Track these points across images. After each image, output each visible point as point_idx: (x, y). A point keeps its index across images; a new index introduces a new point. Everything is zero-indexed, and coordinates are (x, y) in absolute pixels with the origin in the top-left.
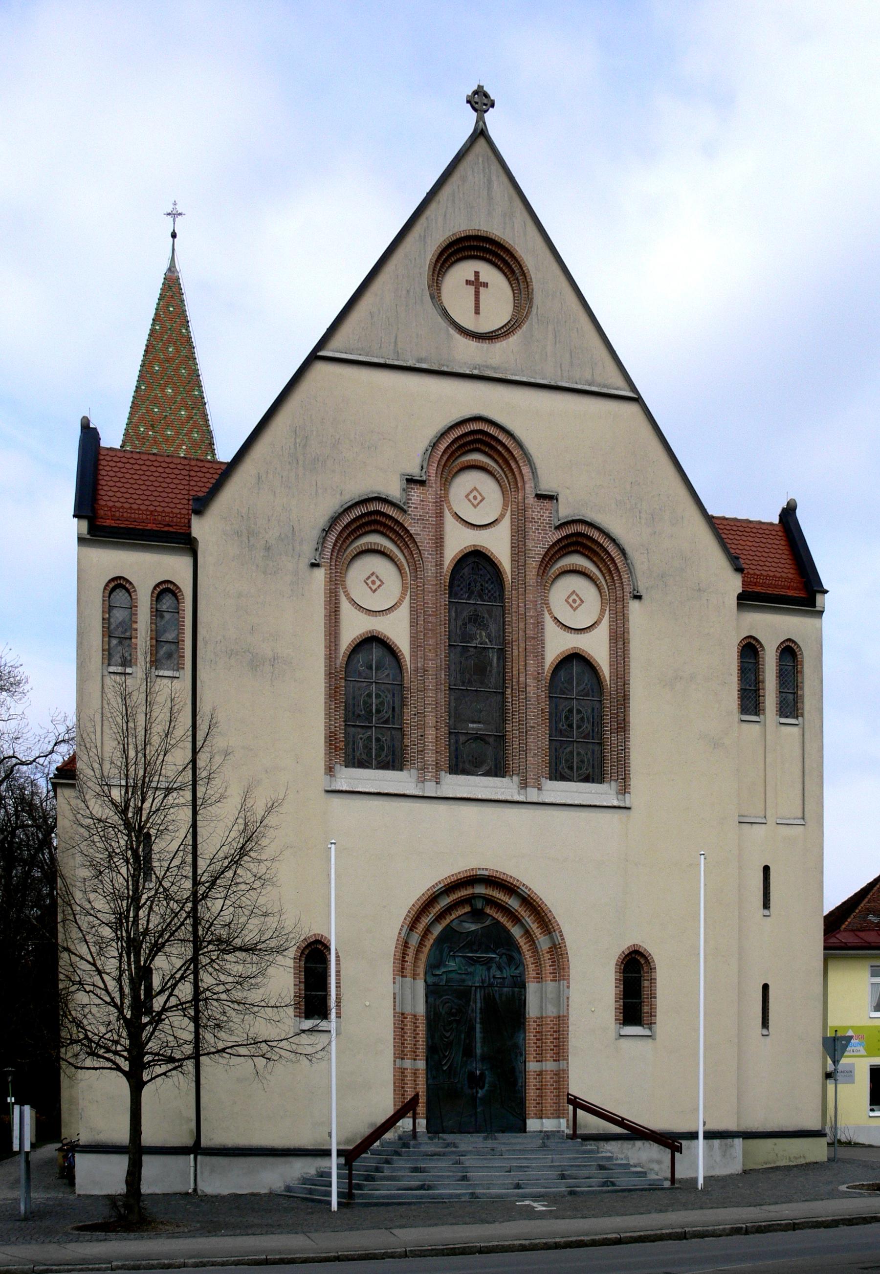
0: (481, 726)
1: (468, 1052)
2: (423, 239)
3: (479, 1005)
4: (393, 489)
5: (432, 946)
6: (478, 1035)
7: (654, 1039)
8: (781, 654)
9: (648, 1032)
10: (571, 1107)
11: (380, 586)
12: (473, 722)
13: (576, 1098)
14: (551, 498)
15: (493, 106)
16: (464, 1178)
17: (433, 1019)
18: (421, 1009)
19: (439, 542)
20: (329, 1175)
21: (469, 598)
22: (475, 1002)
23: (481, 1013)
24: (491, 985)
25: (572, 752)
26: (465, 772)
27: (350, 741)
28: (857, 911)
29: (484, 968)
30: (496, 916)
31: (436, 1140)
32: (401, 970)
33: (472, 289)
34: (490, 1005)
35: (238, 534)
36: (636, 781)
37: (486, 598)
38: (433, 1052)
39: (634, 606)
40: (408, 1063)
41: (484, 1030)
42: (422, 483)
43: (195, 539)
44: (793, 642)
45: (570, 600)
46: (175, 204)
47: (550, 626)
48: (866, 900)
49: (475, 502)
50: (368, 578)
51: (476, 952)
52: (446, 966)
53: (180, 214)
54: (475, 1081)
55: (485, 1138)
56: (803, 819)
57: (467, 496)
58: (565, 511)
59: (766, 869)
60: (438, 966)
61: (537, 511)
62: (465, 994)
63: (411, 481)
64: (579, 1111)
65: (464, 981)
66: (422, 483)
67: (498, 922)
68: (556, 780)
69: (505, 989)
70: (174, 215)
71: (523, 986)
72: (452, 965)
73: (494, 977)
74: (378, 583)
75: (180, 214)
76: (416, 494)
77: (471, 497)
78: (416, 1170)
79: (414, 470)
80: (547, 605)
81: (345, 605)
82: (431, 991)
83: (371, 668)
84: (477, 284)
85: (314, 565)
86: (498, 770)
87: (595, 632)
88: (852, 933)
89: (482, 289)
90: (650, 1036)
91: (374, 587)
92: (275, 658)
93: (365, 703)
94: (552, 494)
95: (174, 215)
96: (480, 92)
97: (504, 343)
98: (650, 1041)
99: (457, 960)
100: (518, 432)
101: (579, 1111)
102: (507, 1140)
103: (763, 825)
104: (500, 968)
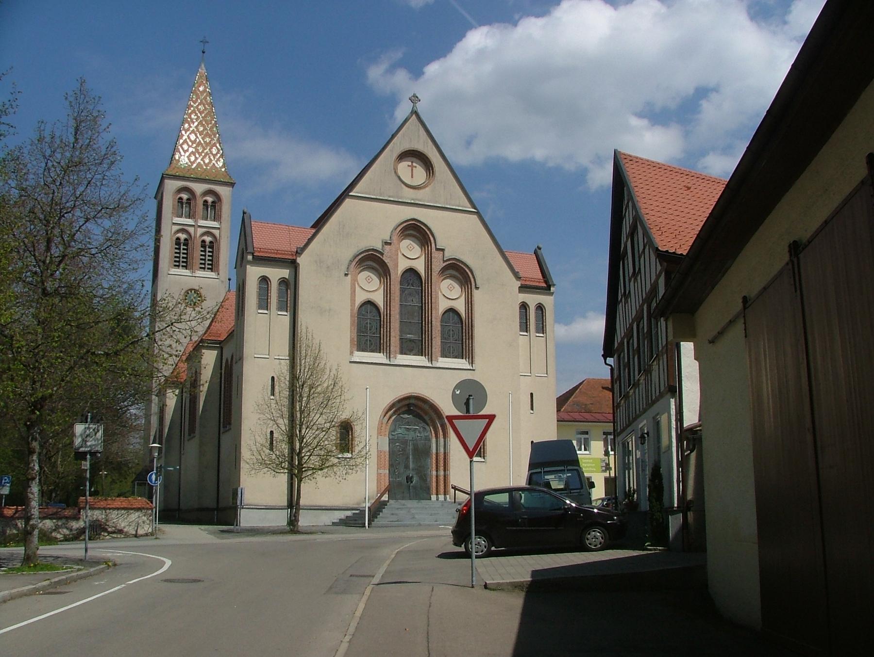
0: (412, 336)
1: (407, 467)
2: (392, 151)
3: (411, 448)
4: (379, 246)
5: (392, 423)
6: (411, 460)
7: (486, 463)
8: (536, 308)
9: (483, 460)
10: (453, 490)
11: (371, 281)
12: (409, 334)
13: (455, 486)
14: (443, 250)
15: (420, 101)
16: (414, 518)
17: (392, 453)
18: (387, 449)
19: (396, 265)
20: (365, 511)
21: (408, 286)
22: (409, 446)
23: (412, 451)
24: (416, 440)
25: (450, 347)
26: (405, 354)
27: (359, 341)
28: (568, 402)
29: (413, 432)
30: (418, 411)
31: (397, 503)
32: (379, 433)
33: (410, 168)
34: (416, 450)
35: (316, 262)
36: (477, 359)
37: (414, 286)
38: (392, 466)
39: (475, 292)
40: (381, 471)
41: (414, 458)
42: (390, 244)
43: (298, 264)
44: (542, 305)
45: (449, 287)
46: (205, 37)
47: (441, 297)
48: (573, 397)
49: (411, 249)
50: (367, 278)
51: (410, 426)
52: (398, 431)
53: (208, 42)
54: (409, 479)
55: (418, 502)
56: (547, 374)
57: (407, 247)
58: (448, 254)
59: (532, 394)
60: (394, 431)
61: (437, 255)
62: (405, 442)
63: (386, 243)
64: (456, 491)
65: (405, 437)
66: (390, 244)
67: (419, 414)
68: (443, 357)
69: (422, 441)
70: (204, 42)
71: (430, 440)
72: (399, 431)
73: (418, 436)
74: (371, 280)
75: (208, 42)
76: (387, 247)
77: (409, 247)
78: (393, 514)
79: (387, 238)
80: (440, 289)
81: (358, 289)
82: (391, 441)
83: (368, 313)
84: (412, 167)
85: (346, 275)
86: (421, 353)
87: (459, 300)
88: (566, 413)
89: (414, 168)
90: (484, 462)
91: (369, 281)
92: (330, 310)
93: (365, 326)
94: (442, 248)
95: (204, 42)
96: (415, 96)
97: (424, 190)
98: (484, 463)
99: (402, 429)
100: (436, 234)
101: (456, 491)
102: (424, 503)
103: (529, 377)
104: (420, 432)
